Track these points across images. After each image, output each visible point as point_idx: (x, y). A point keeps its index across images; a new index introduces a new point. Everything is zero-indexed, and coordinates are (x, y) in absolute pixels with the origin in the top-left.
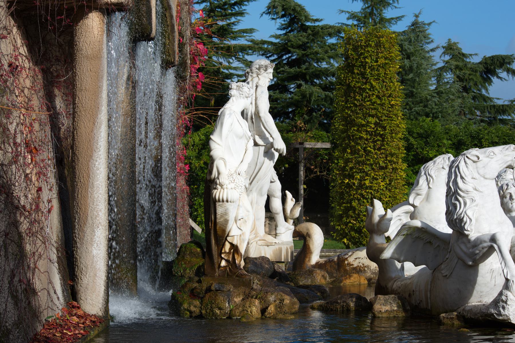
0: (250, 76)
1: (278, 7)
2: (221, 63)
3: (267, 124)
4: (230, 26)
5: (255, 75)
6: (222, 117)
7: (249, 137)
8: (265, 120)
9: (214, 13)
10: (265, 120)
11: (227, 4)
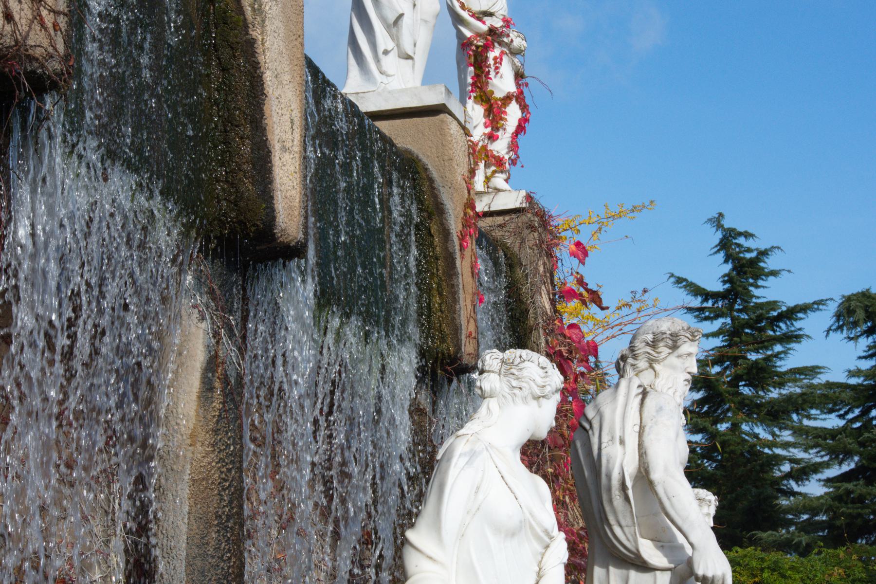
0: (628, 368)
1: (857, 310)
2: (756, 436)
3: (672, 505)
4: (770, 361)
5: (642, 364)
6: (443, 464)
7: (546, 532)
8: (666, 492)
9: (740, 338)
10: (666, 492)
11: (763, 319)
